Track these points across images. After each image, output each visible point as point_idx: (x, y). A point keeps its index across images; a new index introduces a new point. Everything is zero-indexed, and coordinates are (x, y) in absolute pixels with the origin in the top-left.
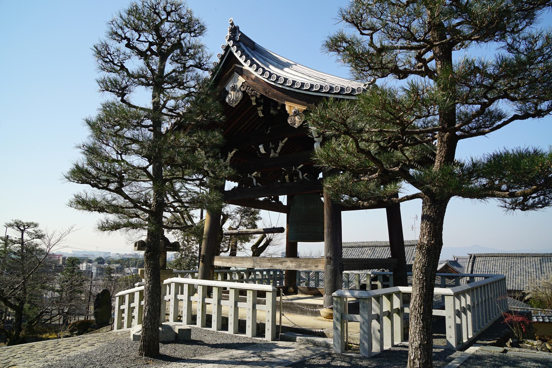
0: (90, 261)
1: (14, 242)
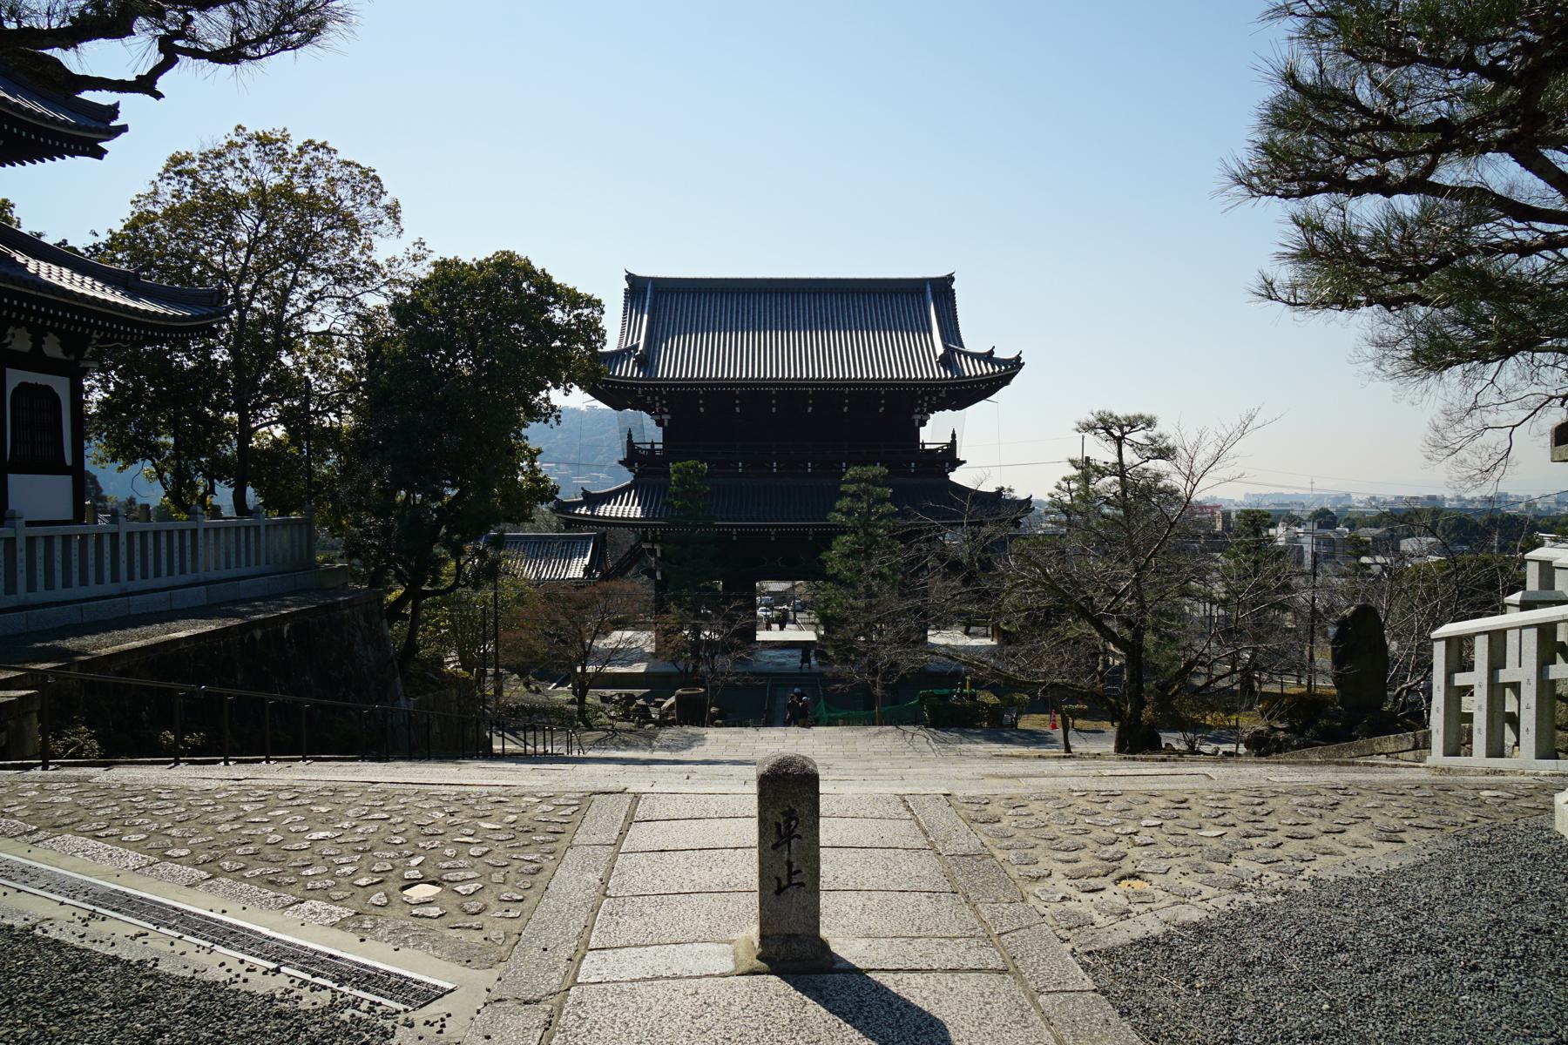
0: (1293, 521)
1: (1102, 473)
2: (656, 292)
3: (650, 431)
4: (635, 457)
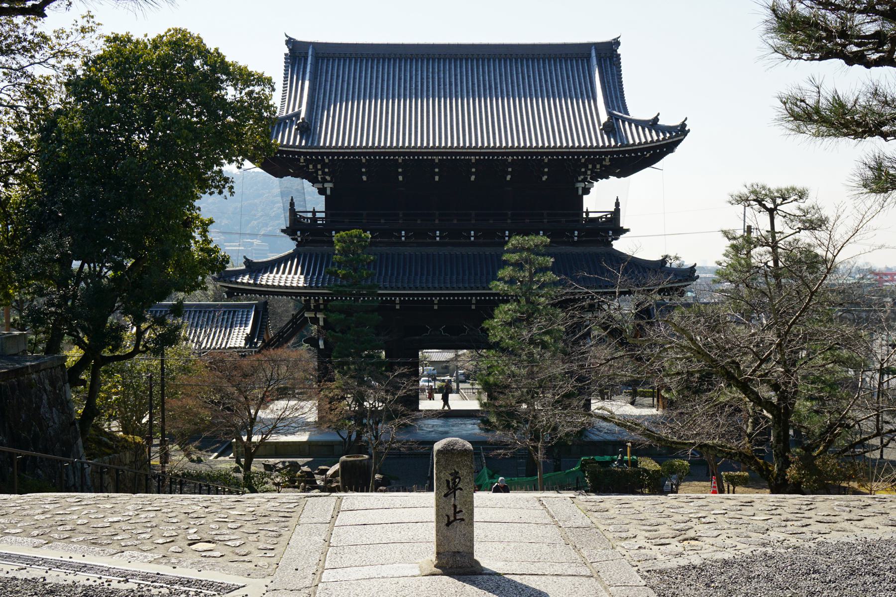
2: (317, 58)
3: (312, 200)
4: (297, 225)
